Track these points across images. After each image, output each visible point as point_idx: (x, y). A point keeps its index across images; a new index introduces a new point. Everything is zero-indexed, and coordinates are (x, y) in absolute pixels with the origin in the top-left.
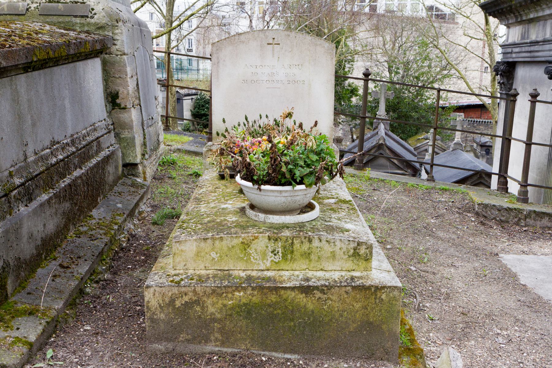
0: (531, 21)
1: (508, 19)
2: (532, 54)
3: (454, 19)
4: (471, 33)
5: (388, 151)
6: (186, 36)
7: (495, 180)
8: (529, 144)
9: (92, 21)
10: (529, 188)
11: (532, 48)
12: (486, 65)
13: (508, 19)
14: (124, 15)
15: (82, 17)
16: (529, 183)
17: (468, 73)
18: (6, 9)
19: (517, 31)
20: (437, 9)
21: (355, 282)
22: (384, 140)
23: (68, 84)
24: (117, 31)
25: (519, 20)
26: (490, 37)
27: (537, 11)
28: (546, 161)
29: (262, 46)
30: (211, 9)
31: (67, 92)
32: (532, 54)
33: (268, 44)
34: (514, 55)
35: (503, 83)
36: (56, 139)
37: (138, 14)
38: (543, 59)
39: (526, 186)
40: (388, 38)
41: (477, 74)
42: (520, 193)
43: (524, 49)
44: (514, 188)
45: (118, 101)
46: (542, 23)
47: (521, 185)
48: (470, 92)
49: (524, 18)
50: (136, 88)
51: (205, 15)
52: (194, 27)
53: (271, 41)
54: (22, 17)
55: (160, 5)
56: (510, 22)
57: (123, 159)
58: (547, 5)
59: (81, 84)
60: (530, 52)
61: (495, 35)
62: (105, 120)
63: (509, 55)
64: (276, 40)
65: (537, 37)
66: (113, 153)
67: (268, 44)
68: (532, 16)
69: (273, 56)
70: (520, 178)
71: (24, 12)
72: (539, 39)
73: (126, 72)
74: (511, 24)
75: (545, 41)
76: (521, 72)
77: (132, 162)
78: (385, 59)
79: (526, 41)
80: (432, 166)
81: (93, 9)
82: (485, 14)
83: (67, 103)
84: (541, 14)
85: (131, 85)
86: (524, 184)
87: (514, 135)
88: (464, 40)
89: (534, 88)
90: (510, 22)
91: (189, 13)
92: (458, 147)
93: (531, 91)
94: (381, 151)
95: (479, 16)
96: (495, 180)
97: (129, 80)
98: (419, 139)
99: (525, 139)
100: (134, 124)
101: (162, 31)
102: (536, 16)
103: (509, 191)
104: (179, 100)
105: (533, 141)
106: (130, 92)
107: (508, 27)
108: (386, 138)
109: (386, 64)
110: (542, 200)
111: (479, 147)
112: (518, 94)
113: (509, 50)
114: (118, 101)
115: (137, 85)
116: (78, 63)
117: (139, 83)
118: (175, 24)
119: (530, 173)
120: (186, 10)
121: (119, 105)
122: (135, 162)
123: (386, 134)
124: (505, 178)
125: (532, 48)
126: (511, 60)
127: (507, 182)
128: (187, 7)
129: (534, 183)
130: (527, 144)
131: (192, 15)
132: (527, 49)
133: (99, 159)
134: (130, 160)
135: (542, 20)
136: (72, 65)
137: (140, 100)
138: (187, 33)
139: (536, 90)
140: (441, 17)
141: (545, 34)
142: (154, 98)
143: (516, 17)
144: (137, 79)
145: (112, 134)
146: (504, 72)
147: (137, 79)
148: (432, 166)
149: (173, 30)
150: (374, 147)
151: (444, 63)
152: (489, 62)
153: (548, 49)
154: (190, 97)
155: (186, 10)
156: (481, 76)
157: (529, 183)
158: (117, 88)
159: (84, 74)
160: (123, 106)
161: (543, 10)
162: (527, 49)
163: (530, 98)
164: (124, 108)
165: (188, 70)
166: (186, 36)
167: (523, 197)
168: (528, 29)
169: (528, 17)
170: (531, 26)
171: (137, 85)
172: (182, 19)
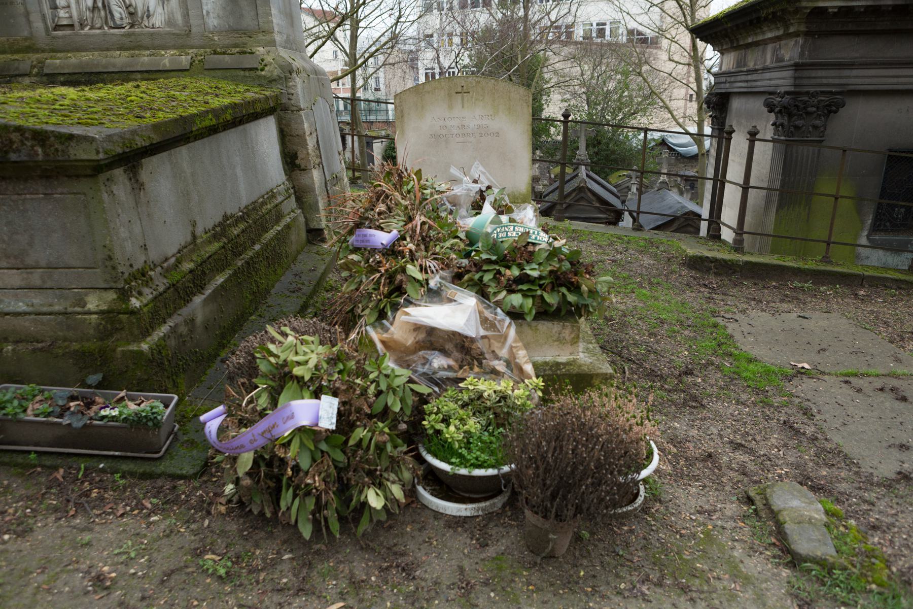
0: (748, 46)
1: (722, 45)
2: (750, 84)
3: (656, 43)
4: (676, 58)
5: (589, 194)
6: (372, 75)
7: (704, 226)
8: (746, 188)
9: (263, 73)
10: (745, 236)
11: (749, 77)
12: (693, 93)
13: (722, 45)
14: (297, 64)
15: (251, 69)
16: (745, 230)
17: (672, 102)
18: (168, 64)
19: (732, 57)
20: (639, 33)
21: (560, 370)
22: (586, 182)
23: (239, 150)
24: (291, 84)
25: (735, 45)
26: (696, 60)
27: (756, 34)
28: (763, 203)
29: (450, 95)
30: (396, 43)
31: (238, 158)
32: (750, 84)
33: (457, 93)
34: (728, 85)
35: (715, 117)
36: (229, 213)
37: (316, 60)
38: (762, 89)
39: (741, 234)
40: (586, 67)
41: (681, 103)
42: (735, 240)
43: (739, 78)
44: (727, 235)
45: (297, 162)
46: (761, 48)
47: (736, 233)
48: (684, 131)
49: (741, 43)
50: (316, 146)
51: (390, 50)
52: (380, 63)
53: (459, 90)
54: (185, 73)
55: (342, 42)
56: (725, 47)
57: (307, 224)
58: (769, 27)
59: (253, 148)
60: (747, 81)
61: (702, 59)
62: (283, 183)
63: (722, 85)
64: (465, 88)
65: (755, 64)
66: (294, 220)
67: (457, 93)
68: (750, 40)
69: (463, 107)
70: (735, 226)
71: (188, 68)
72: (757, 67)
73: (304, 129)
74: (725, 49)
75: (765, 69)
76: (736, 104)
77: (317, 227)
78: (584, 90)
79: (742, 69)
80: (638, 214)
81: (263, 60)
82: (692, 36)
83: (239, 171)
84: (760, 38)
85: (311, 143)
86: (739, 230)
87: (728, 177)
88: (669, 67)
89: (753, 125)
90: (725, 47)
91: (373, 49)
92: (664, 185)
93: (750, 128)
94: (582, 195)
95: (686, 39)
96: (704, 226)
97: (307, 138)
98: (620, 176)
99: (742, 183)
100: (316, 186)
101: (347, 70)
102: (755, 40)
103: (723, 237)
104: (369, 145)
105: (751, 184)
106: (310, 151)
107: (722, 54)
108: (588, 180)
109: (584, 96)
110: (757, 245)
111: (683, 182)
112: (734, 131)
113: (723, 80)
114: (297, 162)
115: (318, 141)
116: (248, 125)
117: (319, 139)
118: (360, 62)
119: (746, 218)
120: (370, 47)
121: (299, 167)
122: (320, 227)
123: (588, 176)
124: (718, 224)
125: (749, 77)
126: (723, 91)
127: (720, 228)
128: (371, 43)
129: (752, 231)
130: (743, 188)
131: (377, 51)
132: (743, 78)
133: (279, 228)
134: (314, 225)
135: (762, 45)
136: (241, 128)
137: (321, 158)
138: (373, 70)
139: (755, 127)
140: (644, 41)
141: (765, 62)
142: (337, 153)
143: (732, 42)
144: (317, 136)
145: (293, 198)
146: (717, 105)
147: (317, 136)
148: (638, 214)
149: (358, 68)
150: (574, 190)
151: (647, 92)
152: (695, 89)
153: (768, 78)
154: (380, 140)
155: (370, 47)
156: (686, 105)
157: (745, 230)
158: (295, 148)
159: (256, 135)
160: (303, 167)
161: (763, 33)
162: (743, 78)
163: (748, 136)
164: (304, 170)
165: (377, 111)
166: (372, 75)
167: (738, 246)
168: (745, 55)
169: (746, 42)
170: (749, 52)
171: (318, 141)
172: (366, 55)
